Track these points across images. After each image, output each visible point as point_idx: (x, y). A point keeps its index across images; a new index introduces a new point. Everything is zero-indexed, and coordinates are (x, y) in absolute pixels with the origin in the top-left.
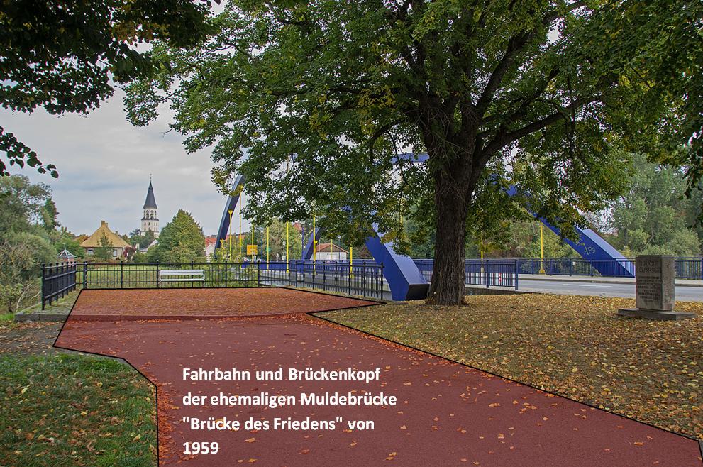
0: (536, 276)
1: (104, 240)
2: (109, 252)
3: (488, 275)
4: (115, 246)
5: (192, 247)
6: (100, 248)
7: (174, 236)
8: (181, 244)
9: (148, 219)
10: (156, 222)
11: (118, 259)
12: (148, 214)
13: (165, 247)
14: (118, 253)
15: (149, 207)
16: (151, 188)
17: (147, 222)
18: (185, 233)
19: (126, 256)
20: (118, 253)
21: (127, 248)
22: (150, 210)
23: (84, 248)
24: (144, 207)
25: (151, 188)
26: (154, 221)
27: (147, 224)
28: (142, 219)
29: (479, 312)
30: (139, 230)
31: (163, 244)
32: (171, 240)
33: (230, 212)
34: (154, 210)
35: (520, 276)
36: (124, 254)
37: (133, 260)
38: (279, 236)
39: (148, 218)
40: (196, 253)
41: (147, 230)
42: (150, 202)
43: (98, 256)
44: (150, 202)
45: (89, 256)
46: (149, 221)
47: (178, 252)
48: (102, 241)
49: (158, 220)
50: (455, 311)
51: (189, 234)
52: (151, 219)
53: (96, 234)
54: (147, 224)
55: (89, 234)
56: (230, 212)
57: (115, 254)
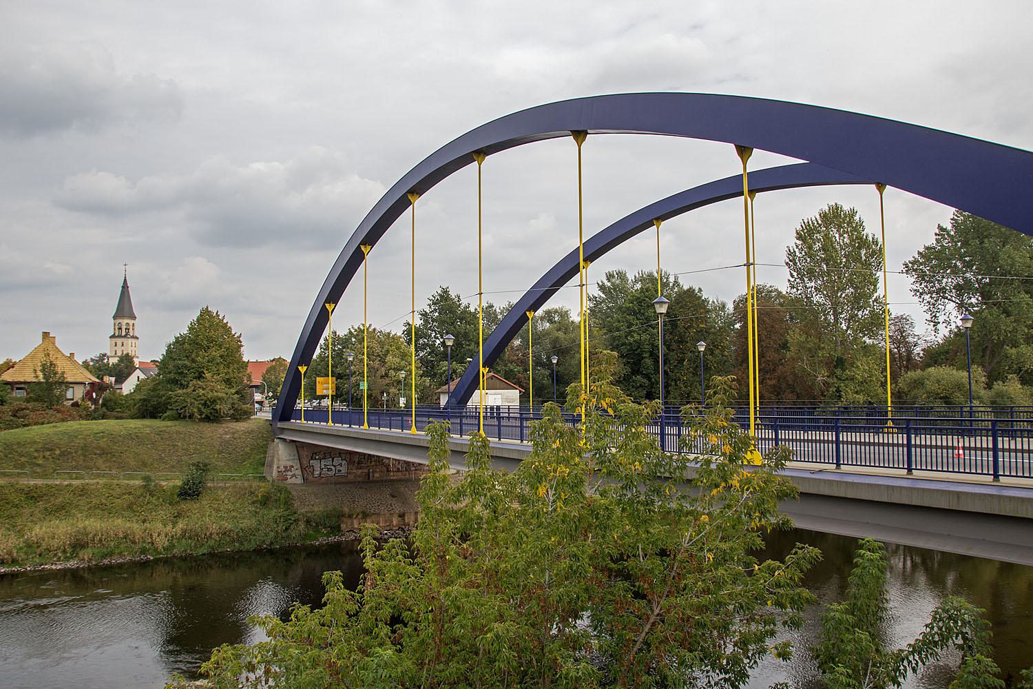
0: (880, 438)
1: (48, 369)
2: (57, 392)
3: (777, 435)
4: (70, 379)
5: (228, 382)
6: (40, 383)
7: (193, 361)
8: (208, 375)
9: (120, 336)
10: (134, 341)
11: (76, 405)
12: (120, 329)
13: (175, 382)
14: (77, 394)
15: (123, 317)
16: (125, 287)
17: (119, 341)
18: (215, 353)
19: (91, 398)
20: (77, 394)
21: (92, 384)
22: (125, 321)
23: (7, 383)
24: (115, 318)
25: (125, 287)
26: (130, 341)
27: (119, 343)
28: (111, 337)
29: (254, 421)
30: (104, 355)
31: (172, 376)
32: (185, 366)
33: (329, 307)
34: (131, 322)
35: (844, 436)
36: (88, 395)
37: (104, 405)
38: (383, 362)
39: (121, 334)
40: (237, 393)
41: (119, 354)
42: (124, 309)
43: (36, 400)
44: (124, 309)
45: (17, 399)
46: (124, 340)
47: (202, 392)
48: (43, 370)
49: (138, 338)
50: (249, 421)
51: (221, 356)
52: (125, 336)
53: (32, 356)
54: (119, 343)
55: (15, 359)
56: (329, 307)
57: (69, 394)
